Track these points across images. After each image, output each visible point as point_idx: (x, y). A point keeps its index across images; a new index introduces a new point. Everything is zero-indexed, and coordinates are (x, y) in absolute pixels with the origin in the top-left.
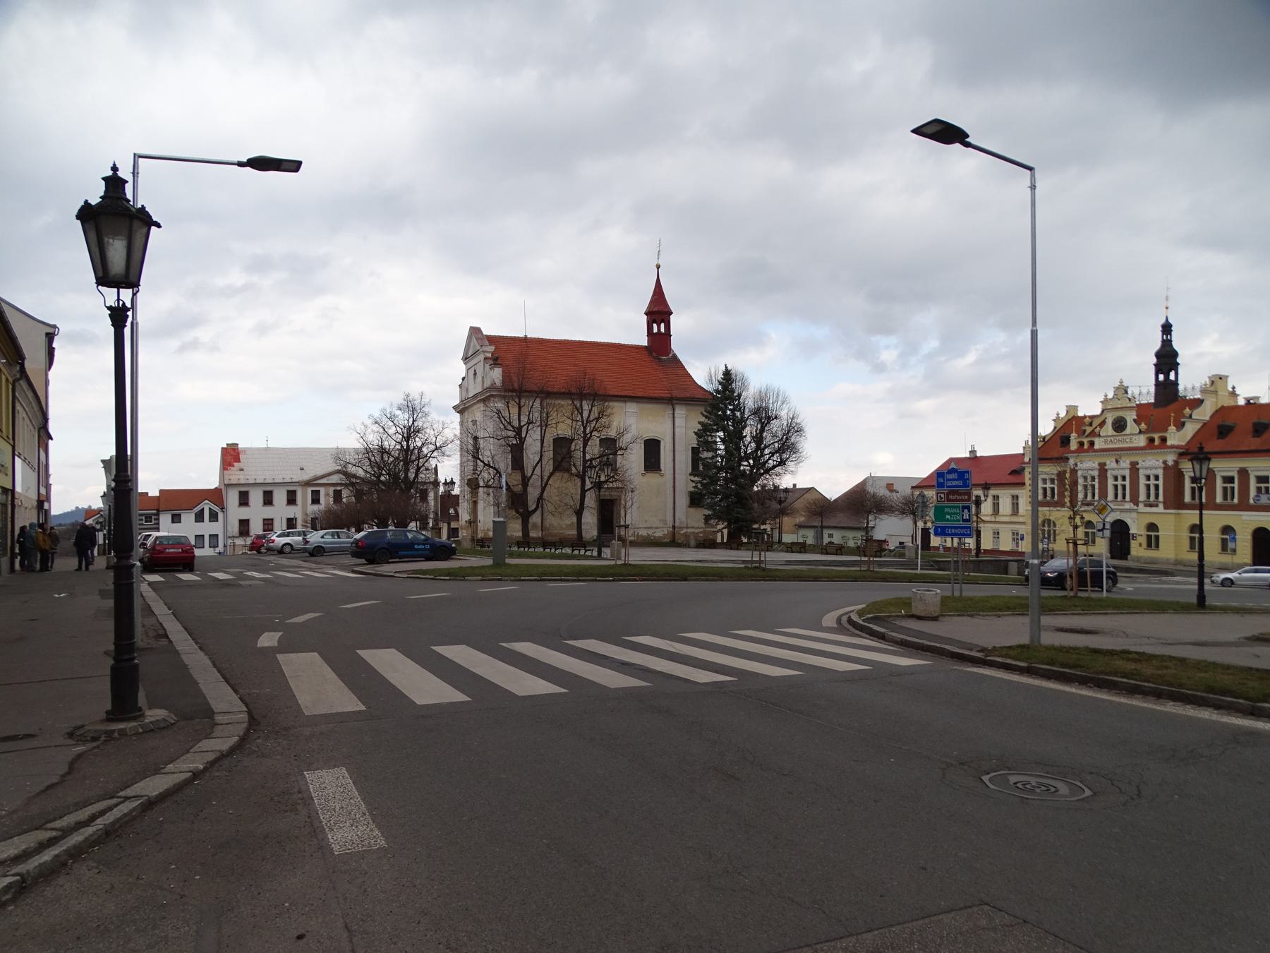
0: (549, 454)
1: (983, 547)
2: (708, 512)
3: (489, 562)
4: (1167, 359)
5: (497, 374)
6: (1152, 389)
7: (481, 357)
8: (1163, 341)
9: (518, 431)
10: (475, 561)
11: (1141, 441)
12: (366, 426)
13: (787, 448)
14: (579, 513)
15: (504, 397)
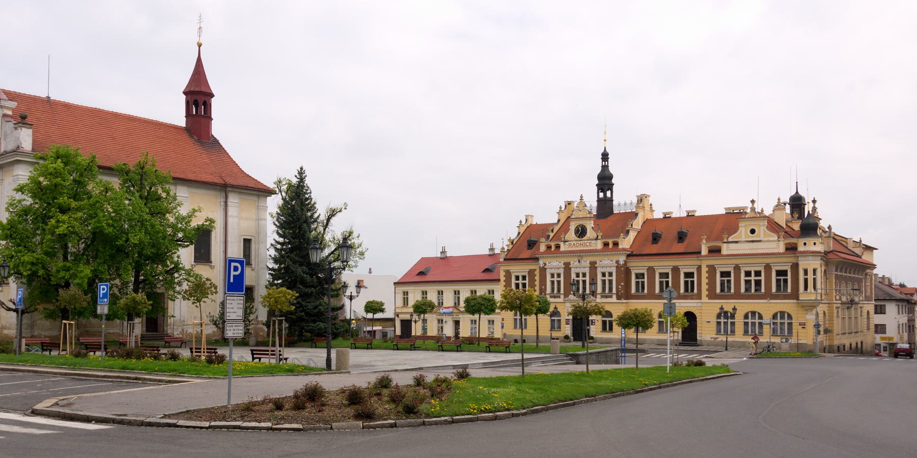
1: (461, 335)
4: (605, 181)
6: (595, 204)
8: (602, 166)
11: (599, 245)
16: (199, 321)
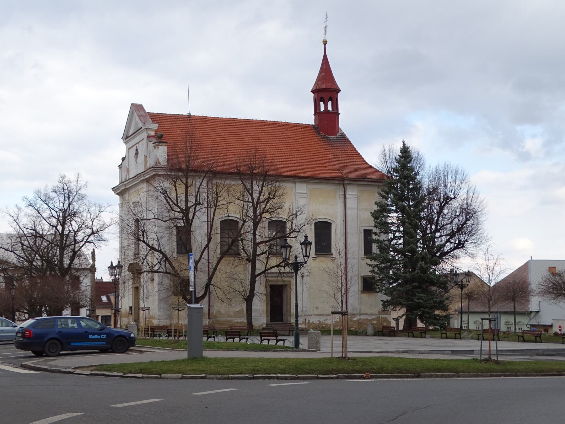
0: (217, 238)
2: (387, 298)
3: (183, 355)
5: (161, 154)
7: (144, 135)
9: (185, 212)
10: (159, 355)
12: (19, 209)
13: (464, 229)
14: (249, 300)
15: (168, 177)
16: (180, 312)
